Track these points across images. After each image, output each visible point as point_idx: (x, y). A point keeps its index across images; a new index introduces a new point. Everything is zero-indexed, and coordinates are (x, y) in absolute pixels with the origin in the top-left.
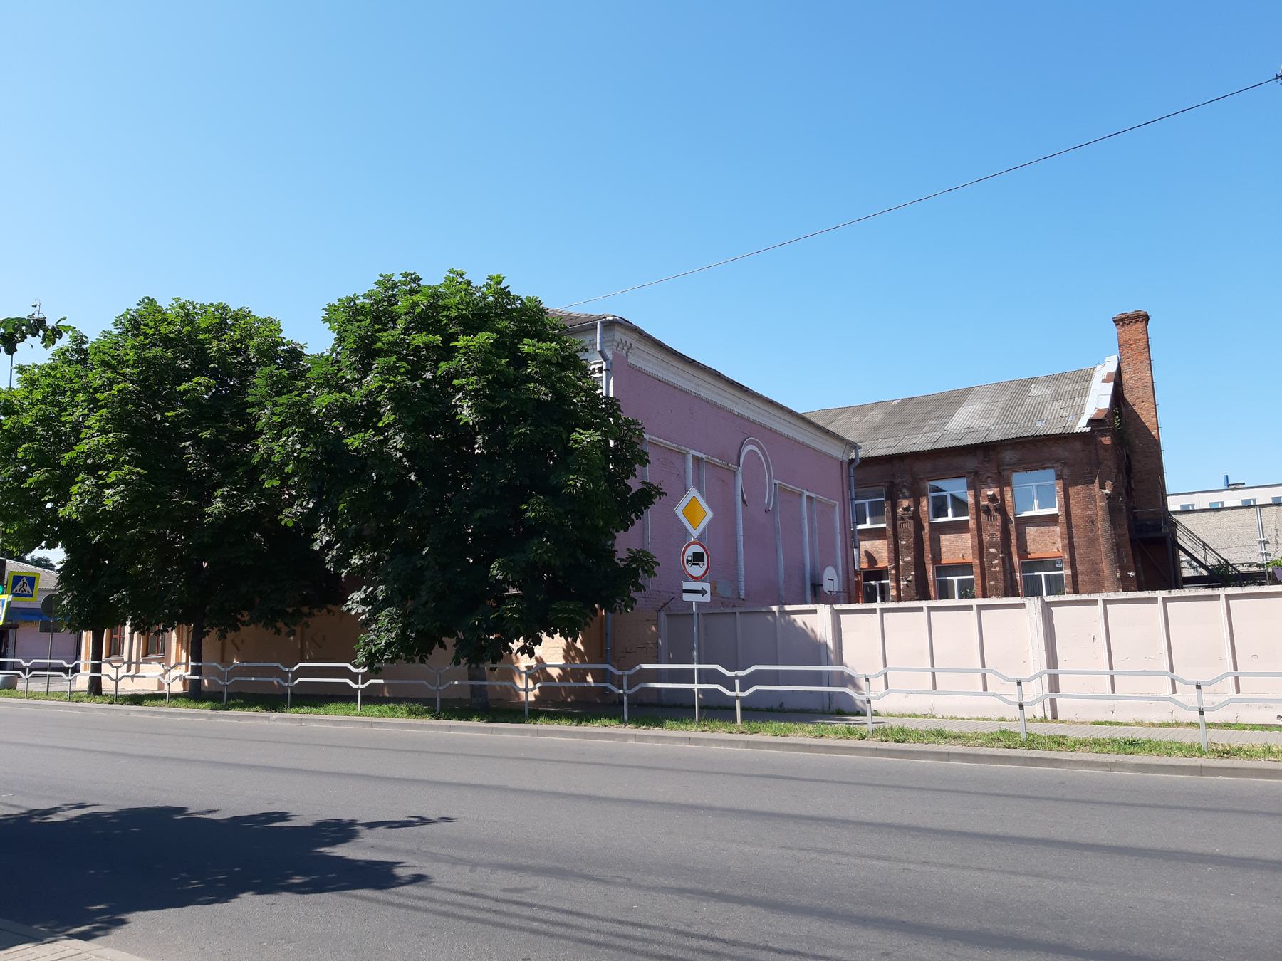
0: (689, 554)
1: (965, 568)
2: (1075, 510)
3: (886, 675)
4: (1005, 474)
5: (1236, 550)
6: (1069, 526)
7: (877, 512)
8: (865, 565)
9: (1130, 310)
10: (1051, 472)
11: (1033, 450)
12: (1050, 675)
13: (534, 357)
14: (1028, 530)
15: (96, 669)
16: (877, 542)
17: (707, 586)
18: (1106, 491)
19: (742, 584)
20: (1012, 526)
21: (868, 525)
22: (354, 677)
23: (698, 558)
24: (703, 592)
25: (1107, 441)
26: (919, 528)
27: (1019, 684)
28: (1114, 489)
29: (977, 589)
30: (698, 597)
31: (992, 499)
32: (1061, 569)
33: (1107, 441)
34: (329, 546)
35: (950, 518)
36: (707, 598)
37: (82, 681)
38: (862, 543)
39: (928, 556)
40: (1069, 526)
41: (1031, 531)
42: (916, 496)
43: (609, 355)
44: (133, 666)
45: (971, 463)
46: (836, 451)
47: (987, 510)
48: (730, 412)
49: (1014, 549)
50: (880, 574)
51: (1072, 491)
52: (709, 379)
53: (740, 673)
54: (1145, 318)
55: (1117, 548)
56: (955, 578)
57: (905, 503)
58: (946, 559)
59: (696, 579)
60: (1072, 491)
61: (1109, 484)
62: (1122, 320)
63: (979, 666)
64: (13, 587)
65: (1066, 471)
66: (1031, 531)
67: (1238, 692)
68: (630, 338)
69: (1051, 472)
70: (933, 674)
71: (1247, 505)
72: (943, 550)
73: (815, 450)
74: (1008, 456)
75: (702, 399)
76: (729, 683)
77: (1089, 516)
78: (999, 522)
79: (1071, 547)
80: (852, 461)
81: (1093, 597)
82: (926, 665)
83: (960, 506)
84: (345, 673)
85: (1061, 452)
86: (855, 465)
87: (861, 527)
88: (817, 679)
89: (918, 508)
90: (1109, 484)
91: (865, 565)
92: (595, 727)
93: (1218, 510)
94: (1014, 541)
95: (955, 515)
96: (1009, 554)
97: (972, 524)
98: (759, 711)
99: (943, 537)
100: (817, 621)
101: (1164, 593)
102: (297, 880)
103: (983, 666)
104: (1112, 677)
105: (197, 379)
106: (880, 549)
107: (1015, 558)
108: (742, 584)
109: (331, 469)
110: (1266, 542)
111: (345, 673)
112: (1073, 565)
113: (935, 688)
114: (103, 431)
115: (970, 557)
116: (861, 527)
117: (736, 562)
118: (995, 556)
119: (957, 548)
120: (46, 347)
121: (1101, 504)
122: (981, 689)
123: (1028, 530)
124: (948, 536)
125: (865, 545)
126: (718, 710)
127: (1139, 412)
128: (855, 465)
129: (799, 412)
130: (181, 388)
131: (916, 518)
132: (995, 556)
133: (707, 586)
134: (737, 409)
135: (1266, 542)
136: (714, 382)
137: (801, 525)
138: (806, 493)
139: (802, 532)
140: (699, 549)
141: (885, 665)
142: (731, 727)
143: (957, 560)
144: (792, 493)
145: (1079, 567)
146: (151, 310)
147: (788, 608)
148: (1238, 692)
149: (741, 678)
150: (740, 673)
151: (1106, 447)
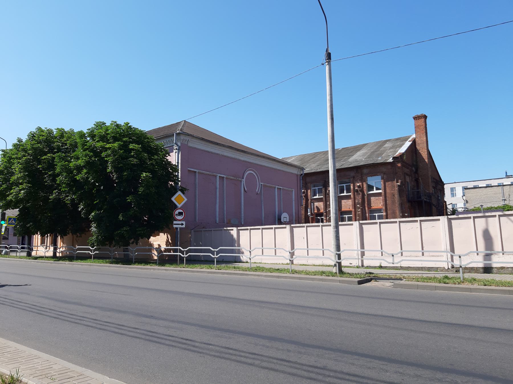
0: (177, 212)
1: (349, 212)
4: (364, 177)
5: (493, 203)
6: (385, 197)
7: (320, 192)
8: (316, 211)
9: (419, 114)
10: (380, 177)
11: (374, 168)
12: (361, 252)
13: (133, 149)
14: (343, 201)
16: (320, 203)
17: (184, 223)
18: (399, 184)
19: (243, 220)
20: (366, 197)
21: (317, 197)
23: (180, 214)
24: (182, 224)
25: (399, 165)
27: (460, 257)
28: (401, 183)
29: (353, 219)
30: (180, 226)
31: (359, 187)
32: (382, 213)
33: (399, 165)
34: (83, 209)
35: (345, 194)
36: (184, 226)
38: (315, 203)
40: (385, 197)
41: (373, 199)
43: (179, 144)
44: (48, 248)
45: (352, 174)
46: (295, 171)
47: (357, 191)
48: (239, 160)
49: (366, 205)
50: (321, 215)
51: (387, 184)
52: (228, 149)
53: (216, 250)
54: (425, 117)
55: (401, 205)
56: (346, 216)
58: (343, 209)
59: (180, 220)
60: (387, 184)
61: (400, 181)
62: (416, 118)
63: (421, 249)
64: (9, 221)
65: (385, 176)
66: (373, 199)
67: (323, 255)
68: (187, 138)
69: (380, 177)
70: (323, 251)
71: (488, 186)
72: (343, 206)
73: (283, 171)
74: (365, 171)
75: (225, 156)
76: (213, 253)
77: (392, 193)
78: (361, 196)
79: (386, 205)
80: (302, 174)
81: (304, 225)
82: (262, 246)
83: (348, 191)
84: (88, 249)
85: (384, 169)
86: (302, 176)
87: (315, 197)
88: (232, 251)
89: (300, 194)
90: (400, 181)
91: (316, 211)
93: (477, 188)
95: (347, 193)
96: (365, 207)
97: (352, 196)
98: (192, 261)
99: (343, 201)
100: (234, 232)
103: (275, 247)
104: (308, 251)
105: (49, 155)
107: (366, 208)
108: (243, 220)
109: (74, 185)
110: (505, 200)
111: (88, 249)
112: (386, 211)
113: (263, 254)
114: (20, 172)
115: (351, 209)
116: (315, 197)
117: (240, 212)
118: (359, 208)
119: (377, 203)
120: (58, 129)
121: (397, 189)
122: (274, 254)
124: (344, 201)
125: (316, 204)
126: (209, 261)
127: (422, 153)
128: (302, 176)
129: (279, 156)
130: (43, 158)
131: (306, 196)
132: (359, 208)
133: (184, 223)
134: (242, 159)
135: (505, 200)
136: (230, 150)
138: (277, 187)
140: (181, 211)
141: (401, 249)
142: (181, 266)
144: (271, 187)
145: (389, 212)
146: (40, 130)
147: (229, 228)
148: (323, 255)
149: (216, 251)
150: (216, 250)
151: (399, 168)
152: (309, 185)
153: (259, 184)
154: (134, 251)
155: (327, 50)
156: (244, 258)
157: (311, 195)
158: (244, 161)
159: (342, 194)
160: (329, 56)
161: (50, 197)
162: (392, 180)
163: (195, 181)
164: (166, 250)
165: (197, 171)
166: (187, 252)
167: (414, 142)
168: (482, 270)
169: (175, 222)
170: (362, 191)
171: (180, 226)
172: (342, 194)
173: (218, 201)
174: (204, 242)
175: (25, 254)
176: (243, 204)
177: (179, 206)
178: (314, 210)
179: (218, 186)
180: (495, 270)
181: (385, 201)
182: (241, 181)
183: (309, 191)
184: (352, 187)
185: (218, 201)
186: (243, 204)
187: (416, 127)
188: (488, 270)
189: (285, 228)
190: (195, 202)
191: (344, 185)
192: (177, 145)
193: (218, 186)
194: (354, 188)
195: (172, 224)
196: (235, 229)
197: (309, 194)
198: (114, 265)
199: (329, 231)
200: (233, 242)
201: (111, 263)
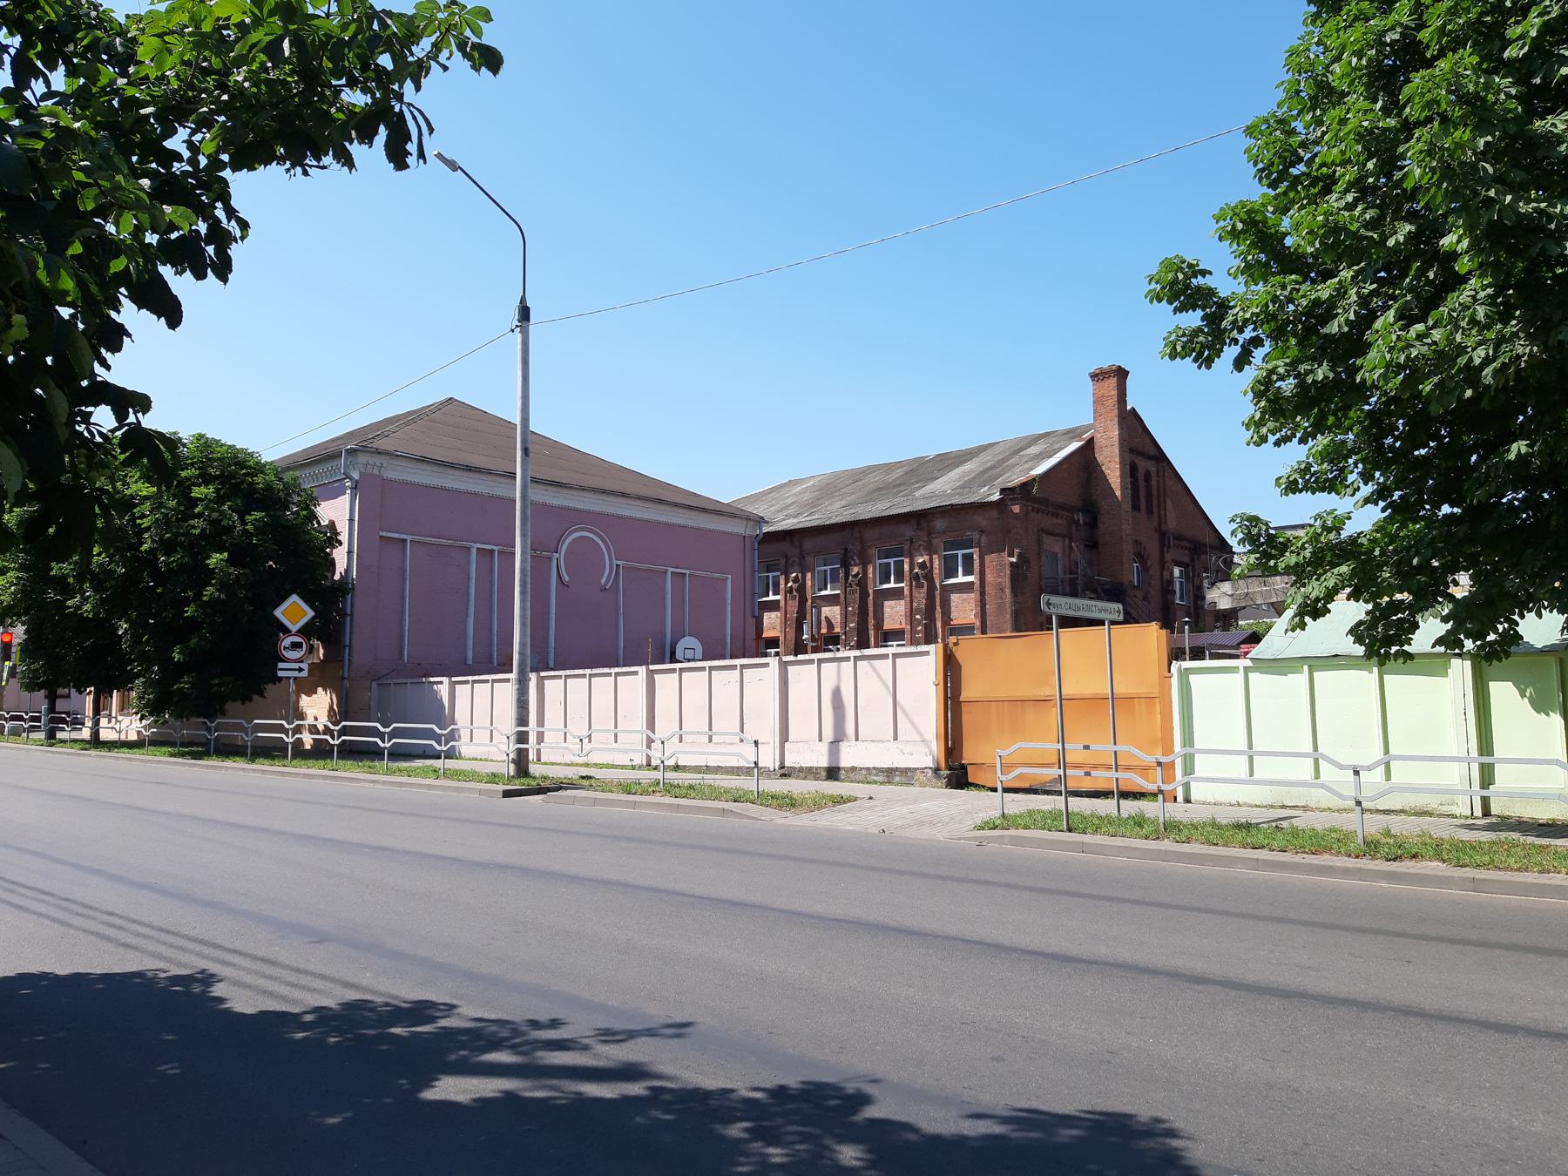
0: (287, 642)
2: (989, 578)
3: (1388, 765)
8: (824, 631)
9: (1105, 365)
12: (1482, 766)
14: (953, 596)
15: (96, 723)
19: (552, 655)
21: (827, 592)
22: (381, 736)
25: (1016, 509)
26: (864, 595)
27: (1357, 773)
28: (1020, 555)
30: (296, 674)
33: (1016, 509)
35: (892, 585)
36: (305, 674)
37: (86, 734)
39: (871, 622)
41: (954, 597)
42: (864, 564)
43: (356, 476)
45: (907, 531)
46: (738, 528)
49: (938, 616)
54: (1121, 374)
57: (855, 570)
59: (296, 661)
66: (955, 598)
68: (377, 460)
78: (925, 590)
82: (596, 718)
83: (899, 579)
84: (281, 729)
85: (981, 520)
87: (824, 593)
92: (229, 763)
94: (871, 614)
97: (906, 592)
99: (886, 603)
100: (443, 686)
101: (588, 671)
102: (833, 1102)
106: (832, 612)
107: (939, 624)
108: (552, 655)
111: (281, 729)
116: (824, 593)
123: (953, 596)
125: (826, 611)
126: (373, 753)
131: (862, 583)
132: (919, 622)
134: (555, 502)
137: (664, 600)
139: (664, 606)
140: (298, 639)
141: (1387, 751)
143: (897, 626)
151: (1016, 516)
152: (809, 559)
153: (609, 562)
154: (266, 727)
155: (523, 299)
156: (465, 748)
157: (813, 585)
158: (559, 508)
159: (885, 586)
160: (525, 314)
161: (69, 603)
162: (1000, 550)
163: (404, 561)
164: (327, 731)
165: (409, 538)
166: (392, 735)
167: (1091, 442)
168: (824, 774)
169: (281, 665)
170: (929, 577)
171: (296, 674)
172: (885, 586)
173: (472, 609)
174: (385, 716)
175: (42, 735)
176: (553, 615)
177: (294, 628)
178: (819, 628)
179: (473, 574)
180: (843, 774)
181: (983, 603)
182: (550, 559)
183: (809, 576)
184: (906, 567)
185: (472, 609)
186: (553, 615)
187: (1098, 401)
188: (833, 773)
189: (636, 673)
190: (403, 613)
191: (891, 561)
192: (351, 479)
193: (473, 574)
194: (912, 569)
195: (275, 669)
196: (445, 680)
197: (809, 583)
198: (180, 760)
199: (505, 691)
200: (441, 715)
201: (172, 755)
